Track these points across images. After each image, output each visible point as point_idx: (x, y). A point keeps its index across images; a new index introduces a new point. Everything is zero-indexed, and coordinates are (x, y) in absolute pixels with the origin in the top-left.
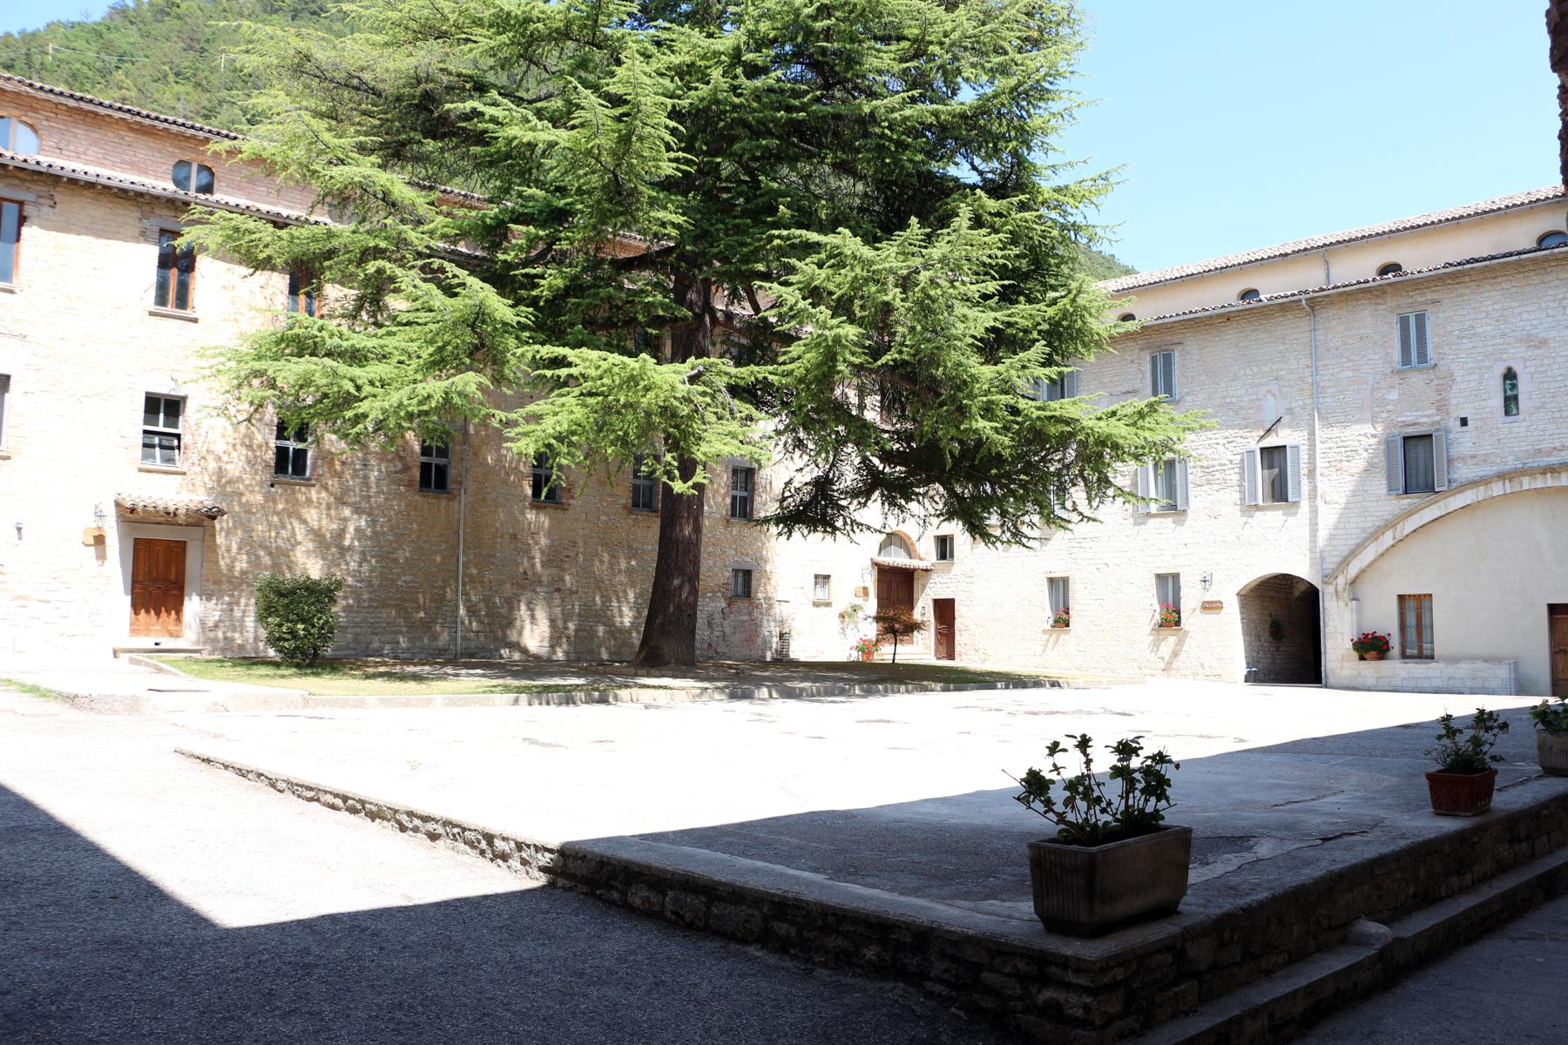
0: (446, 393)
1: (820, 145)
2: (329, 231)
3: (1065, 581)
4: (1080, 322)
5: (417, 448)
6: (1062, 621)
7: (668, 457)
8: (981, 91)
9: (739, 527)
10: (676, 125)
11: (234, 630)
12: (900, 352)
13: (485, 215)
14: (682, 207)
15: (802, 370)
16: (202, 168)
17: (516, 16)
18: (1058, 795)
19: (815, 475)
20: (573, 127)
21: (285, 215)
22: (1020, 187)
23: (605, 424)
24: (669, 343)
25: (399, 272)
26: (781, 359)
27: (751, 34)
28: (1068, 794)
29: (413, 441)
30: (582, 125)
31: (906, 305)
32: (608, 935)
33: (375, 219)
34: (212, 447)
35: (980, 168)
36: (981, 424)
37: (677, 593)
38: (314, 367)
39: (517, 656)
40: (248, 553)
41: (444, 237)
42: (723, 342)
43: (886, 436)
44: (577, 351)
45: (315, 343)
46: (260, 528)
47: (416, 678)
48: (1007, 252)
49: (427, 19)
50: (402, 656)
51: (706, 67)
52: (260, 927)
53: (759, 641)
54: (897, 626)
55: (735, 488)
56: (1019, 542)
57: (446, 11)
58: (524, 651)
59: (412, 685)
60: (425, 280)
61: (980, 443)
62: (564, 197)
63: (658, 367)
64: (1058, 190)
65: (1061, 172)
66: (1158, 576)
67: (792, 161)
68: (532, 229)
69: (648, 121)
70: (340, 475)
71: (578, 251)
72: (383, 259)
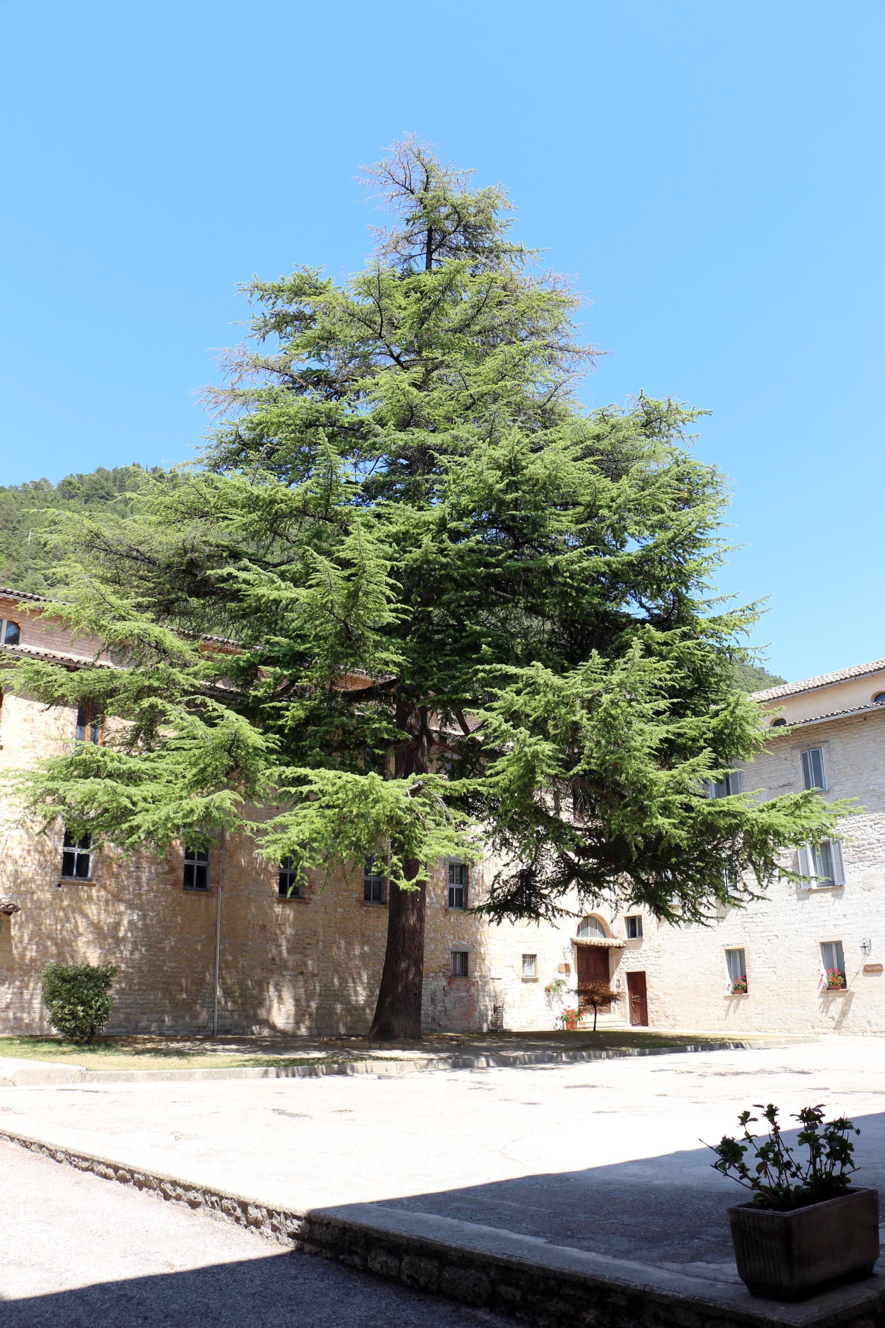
0: (207, 808)
1: (514, 593)
2: (112, 673)
3: (741, 952)
4: (739, 731)
5: (182, 852)
6: (741, 988)
7: (395, 859)
8: (645, 543)
9: (455, 916)
10: (394, 582)
11: (23, 1010)
12: (589, 763)
13: (239, 659)
14: (402, 648)
15: (507, 781)
16: (11, 623)
17: (264, 499)
18: (750, 1159)
19: (520, 868)
20: (310, 586)
21: (75, 660)
22: (682, 620)
23: (340, 832)
24: (392, 760)
25: (169, 707)
26: (488, 773)
27: (453, 506)
28: (760, 1160)
29: (177, 844)
30: (318, 585)
31: (592, 723)
32: (351, 1300)
33: (149, 664)
34: (10, 852)
35: (647, 605)
36: (661, 821)
37: (404, 975)
38: (98, 787)
39: (266, 1032)
40: (37, 944)
41: (206, 677)
42: (438, 759)
43: (579, 833)
44: (317, 771)
45: (98, 767)
46: (48, 922)
47: (179, 1053)
48: (674, 675)
49: (193, 502)
50: (167, 1033)
51: (418, 534)
52: (35, 1299)
53: (477, 1014)
54: (596, 998)
55: (451, 881)
56: (699, 921)
57: (208, 496)
58: (273, 1027)
59: (175, 1060)
60: (190, 713)
61: (660, 836)
62: (304, 642)
63: (384, 783)
64: (713, 621)
65: (715, 606)
66: (823, 945)
67: (490, 606)
68: (278, 669)
69: (372, 579)
70: (117, 876)
71: (316, 686)
72: (156, 696)
